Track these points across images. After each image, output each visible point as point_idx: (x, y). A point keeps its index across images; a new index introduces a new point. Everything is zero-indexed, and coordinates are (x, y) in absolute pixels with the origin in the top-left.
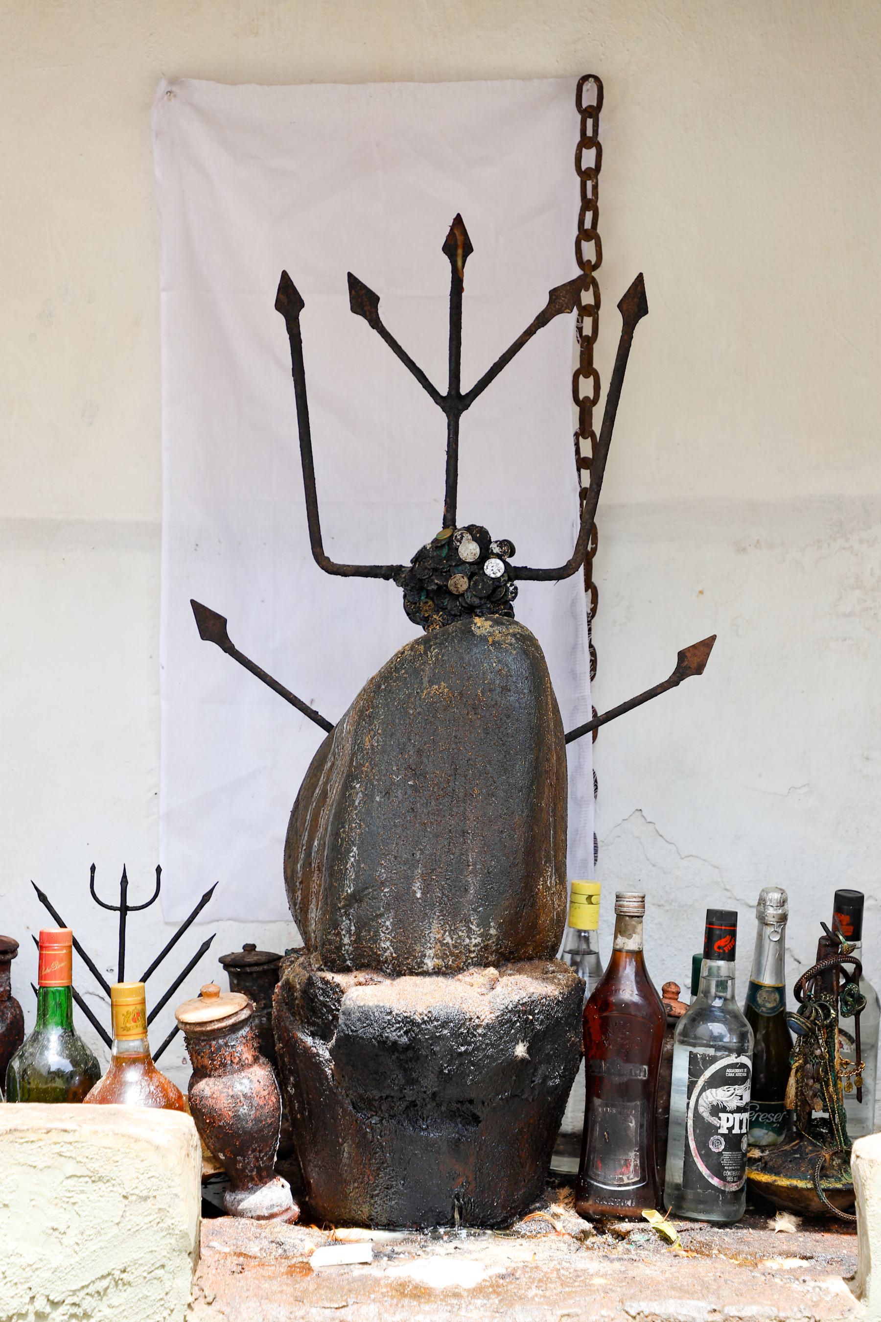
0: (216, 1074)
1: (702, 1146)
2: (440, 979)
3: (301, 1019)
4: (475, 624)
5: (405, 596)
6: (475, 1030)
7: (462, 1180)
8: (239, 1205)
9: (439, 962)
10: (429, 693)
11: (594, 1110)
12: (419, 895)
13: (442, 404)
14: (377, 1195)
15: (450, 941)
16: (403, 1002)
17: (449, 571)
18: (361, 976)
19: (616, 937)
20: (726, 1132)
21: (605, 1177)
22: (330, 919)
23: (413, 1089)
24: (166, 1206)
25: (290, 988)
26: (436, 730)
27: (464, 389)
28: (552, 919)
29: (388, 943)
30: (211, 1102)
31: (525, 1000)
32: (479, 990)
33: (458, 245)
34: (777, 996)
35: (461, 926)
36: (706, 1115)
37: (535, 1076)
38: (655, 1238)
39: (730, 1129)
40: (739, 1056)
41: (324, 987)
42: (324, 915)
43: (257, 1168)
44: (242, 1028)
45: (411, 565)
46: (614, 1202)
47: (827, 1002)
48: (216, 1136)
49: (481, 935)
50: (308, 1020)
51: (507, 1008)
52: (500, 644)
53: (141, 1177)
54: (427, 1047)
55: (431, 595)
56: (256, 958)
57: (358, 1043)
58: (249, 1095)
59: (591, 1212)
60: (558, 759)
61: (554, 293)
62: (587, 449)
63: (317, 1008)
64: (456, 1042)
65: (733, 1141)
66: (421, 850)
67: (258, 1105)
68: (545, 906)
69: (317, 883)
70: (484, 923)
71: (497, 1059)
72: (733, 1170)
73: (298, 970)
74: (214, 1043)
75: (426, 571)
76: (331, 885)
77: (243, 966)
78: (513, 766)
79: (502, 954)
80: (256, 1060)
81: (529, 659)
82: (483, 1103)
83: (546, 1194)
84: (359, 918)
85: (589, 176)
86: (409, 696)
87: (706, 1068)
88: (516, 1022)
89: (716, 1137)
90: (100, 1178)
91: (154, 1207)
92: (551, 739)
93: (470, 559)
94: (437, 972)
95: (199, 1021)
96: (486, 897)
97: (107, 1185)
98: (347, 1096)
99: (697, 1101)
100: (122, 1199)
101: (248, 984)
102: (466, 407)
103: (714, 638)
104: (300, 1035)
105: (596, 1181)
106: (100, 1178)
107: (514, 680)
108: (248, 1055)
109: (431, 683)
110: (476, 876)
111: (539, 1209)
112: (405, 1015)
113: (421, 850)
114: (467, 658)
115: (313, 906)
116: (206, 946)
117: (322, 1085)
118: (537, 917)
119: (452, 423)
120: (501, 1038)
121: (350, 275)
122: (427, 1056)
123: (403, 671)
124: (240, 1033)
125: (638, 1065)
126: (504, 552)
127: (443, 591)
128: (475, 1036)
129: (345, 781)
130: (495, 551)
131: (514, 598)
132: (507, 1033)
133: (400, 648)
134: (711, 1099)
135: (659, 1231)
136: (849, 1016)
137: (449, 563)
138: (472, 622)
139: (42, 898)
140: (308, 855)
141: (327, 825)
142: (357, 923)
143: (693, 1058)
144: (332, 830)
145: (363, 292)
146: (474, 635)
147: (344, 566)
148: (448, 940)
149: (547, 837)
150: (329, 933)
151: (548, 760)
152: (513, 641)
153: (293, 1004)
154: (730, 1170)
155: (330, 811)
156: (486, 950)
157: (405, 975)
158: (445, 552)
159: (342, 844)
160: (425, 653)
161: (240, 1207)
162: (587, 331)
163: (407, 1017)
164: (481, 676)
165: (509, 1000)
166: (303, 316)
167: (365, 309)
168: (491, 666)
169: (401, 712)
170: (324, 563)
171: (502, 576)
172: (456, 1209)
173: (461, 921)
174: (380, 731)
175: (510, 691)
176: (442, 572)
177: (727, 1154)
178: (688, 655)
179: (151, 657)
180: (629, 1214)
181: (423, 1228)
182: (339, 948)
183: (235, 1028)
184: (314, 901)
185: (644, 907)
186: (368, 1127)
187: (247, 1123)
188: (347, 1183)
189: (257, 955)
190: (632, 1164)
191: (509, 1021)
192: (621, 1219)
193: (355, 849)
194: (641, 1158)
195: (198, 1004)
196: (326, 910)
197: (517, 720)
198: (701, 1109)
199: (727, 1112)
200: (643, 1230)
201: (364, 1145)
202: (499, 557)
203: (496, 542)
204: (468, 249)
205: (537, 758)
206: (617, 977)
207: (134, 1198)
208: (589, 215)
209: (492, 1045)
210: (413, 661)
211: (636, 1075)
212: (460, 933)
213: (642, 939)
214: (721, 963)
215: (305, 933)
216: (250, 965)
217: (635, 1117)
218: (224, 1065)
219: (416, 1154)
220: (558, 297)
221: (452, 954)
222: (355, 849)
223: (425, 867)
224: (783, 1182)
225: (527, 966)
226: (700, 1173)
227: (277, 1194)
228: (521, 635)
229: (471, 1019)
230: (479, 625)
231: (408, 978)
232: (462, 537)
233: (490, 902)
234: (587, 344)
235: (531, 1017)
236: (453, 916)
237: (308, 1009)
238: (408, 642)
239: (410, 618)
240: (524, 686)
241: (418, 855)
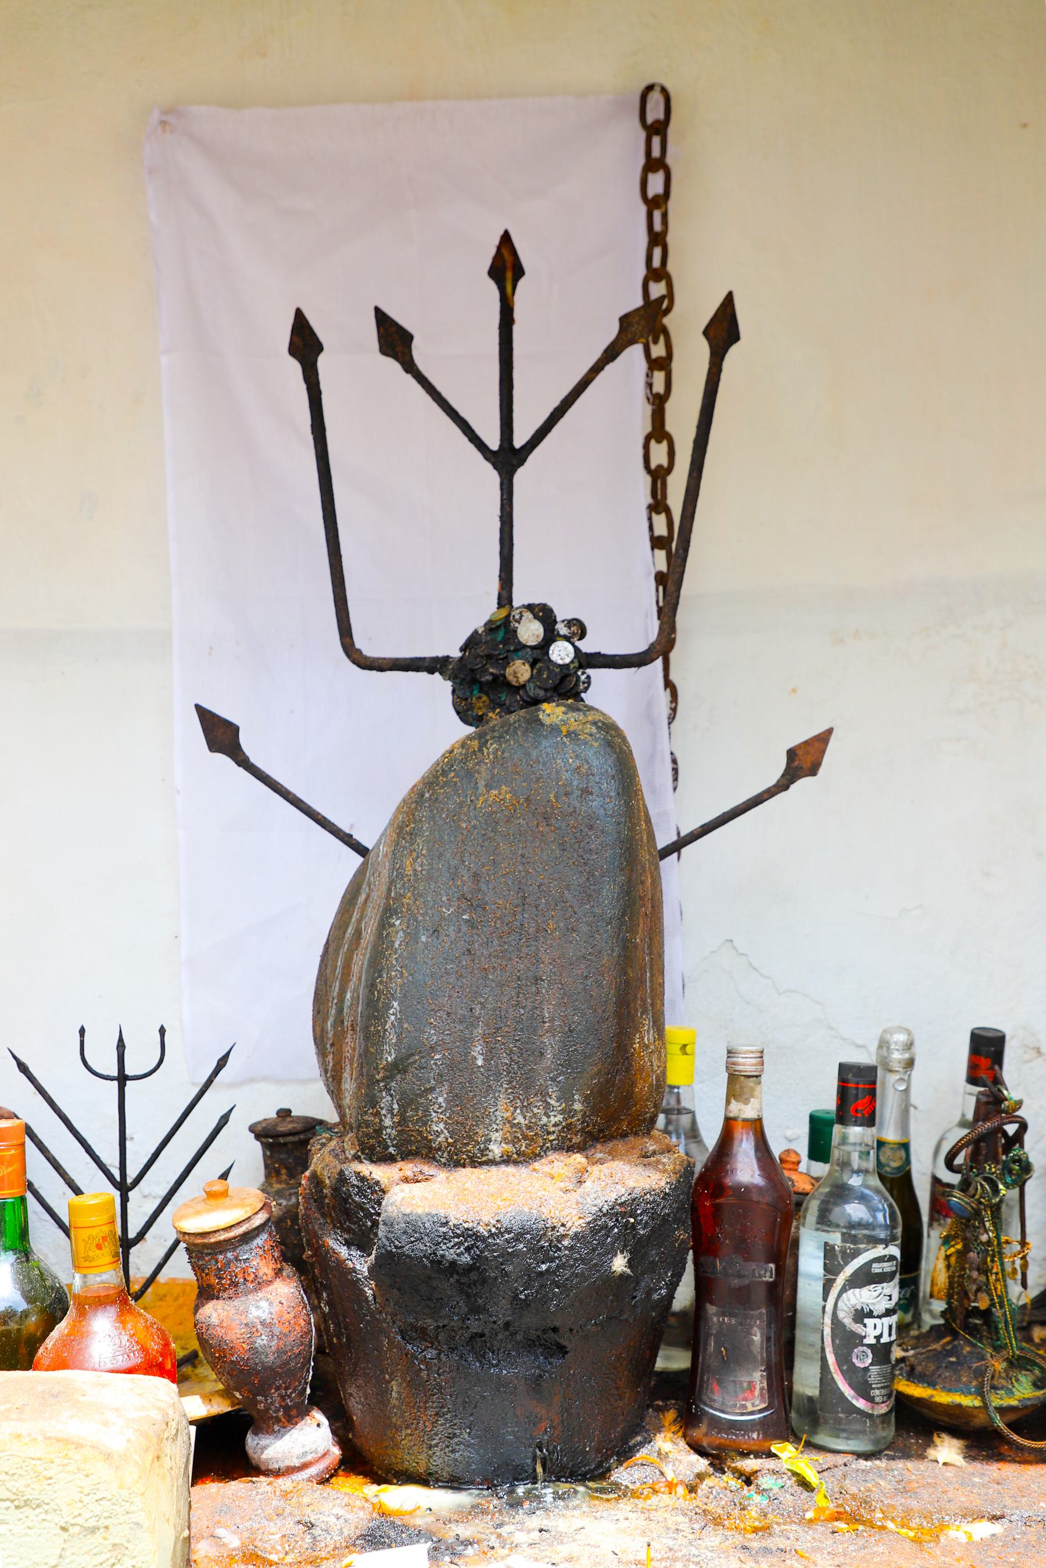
0: (226, 1295)
2: (510, 1169)
3: (332, 1222)
4: (544, 711)
5: (454, 692)
6: (560, 1242)
7: (545, 1424)
8: (262, 1453)
9: (509, 1148)
10: (486, 800)
14: (436, 1445)
15: (522, 1121)
16: (463, 1208)
17: (506, 657)
18: (409, 1168)
19: (728, 1102)
20: (873, 1341)
21: (723, 1404)
22: (367, 1095)
23: (479, 1319)
24: (123, 1541)
25: (318, 1183)
26: (497, 847)
27: (519, 441)
28: (651, 1085)
29: (442, 1126)
30: (220, 1332)
31: (623, 1199)
32: (562, 1185)
33: (506, 267)
34: (903, 1153)
35: (535, 1100)
36: (848, 1322)
37: (635, 1290)
38: (791, 1482)
39: (878, 1338)
42: (359, 1088)
43: (284, 1408)
44: (258, 1235)
46: (736, 1435)
47: (993, 1173)
49: (563, 1112)
50: (341, 1225)
51: (600, 1210)
52: (576, 735)
53: (86, 1500)
54: (497, 1268)
55: (486, 689)
56: (290, 1126)
58: (268, 1321)
59: (705, 1445)
60: (653, 882)
61: (625, 321)
62: (661, 529)
63: (352, 1211)
65: (881, 1352)
66: (481, 1003)
67: (281, 1333)
68: (642, 1069)
69: (352, 1045)
70: (566, 1096)
72: (882, 1388)
73: (329, 1158)
74: (220, 1257)
75: (478, 660)
76: (367, 1050)
77: (275, 1136)
78: (599, 892)
79: (590, 1133)
80: (278, 1273)
81: (615, 752)
82: (571, 1330)
83: (647, 1419)
84: (403, 1093)
85: (657, 203)
86: (461, 805)
87: (846, 1263)
88: (612, 1228)
89: (861, 1348)
90: (27, 1503)
91: (105, 1542)
92: (644, 856)
93: (532, 642)
94: (507, 1160)
95: (201, 1231)
96: (567, 1064)
97: (38, 1511)
98: (394, 1322)
100: (59, 1531)
101: (282, 1156)
102: (522, 462)
104: (331, 1243)
105: (712, 1408)
106: (27, 1503)
107: (597, 779)
108: (265, 1268)
109: (489, 787)
110: (554, 1036)
111: (641, 1444)
112: (466, 1225)
113: (481, 1003)
114: (534, 753)
115: (346, 1075)
117: (361, 1308)
118: (633, 1084)
119: (505, 481)
120: (594, 1250)
121: (377, 310)
122: (496, 1278)
123: (452, 774)
125: (762, 1264)
127: (500, 683)
128: (559, 1249)
129: (382, 916)
130: (562, 633)
131: (586, 689)
132: (602, 1244)
133: (448, 747)
134: (853, 1301)
135: (795, 1474)
136: (1014, 1188)
137: (507, 648)
139: (23, 1068)
140: (340, 1011)
141: (361, 973)
142: (400, 1100)
143: (829, 1251)
144: (366, 980)
146: (542, 725)
147: (379, 659)
148: (520, 1119)
149: (643, 982)
150: (366, 1112)
151: (642, 882)
152: (594, 730)
153: (322, 1203)
154: (878, 1389)
155: (364, 955)
156: (569, 1130)
157: (464, 1166)
158: (500, 635)
159: (379, 998)
160: (481, 750)
161: (264, 1456)
162: (659, 387)
163: (468, 1229)
164: (554, 776)
165: (604, 1199)
167: (397, 349)
168: (566, 763)
169: (451, 827)
170: (355, 656)
171: (572, 662)
172: (539, 1461)
173: (536, 1095)
174: (424, 852)
175: (592, 793)
176: (498, 659)
177: (874, 1369)
178: (800, 752)
179: (163, 780)
180: (754, 1448)
181: (496, 1486)
182: (379, 1132)
183: (247, 1238)
184: (348, 1068)
187: (266, 1357)
188: (398, 1429)
190: (758, 1387)
191: (604, 1227)
192: (745, 1455)
193: (396, 1004)
195: (200, 1206)
197: (603, 832)
198: (841, 1315)
200: (774, 1472)
201: (415, 1384)
202: (567, 639)
204: (519, 272)
205: (630, 880)
207: (77, 1529)
208: (657, 252)
210: (465, 760)
211: (760, 1276)
212: (535, 1110)
213: (761, 1104)
214: (858, 1129)
216: (284, 1135)
218: (236, 1285)
219: (484, 1397)
220: (630, 324)
221: (525, 1137)
222: (396, 1004)
223: (487, 1025)
224: (943, 1398)
225: (620, 1145)
226: (842, 1394)
227: (311, 1437)
228: (604, 723)
229: (553, 1228)
230: (548, 712)
232: (522, 616)
233: (573, 1068)
234: (658, 403)
235: (632, 1220)
236: (525, 1087)
238: (457, 739)
239: (461, 718)
240: (610, 787)
241: (477, 1010)
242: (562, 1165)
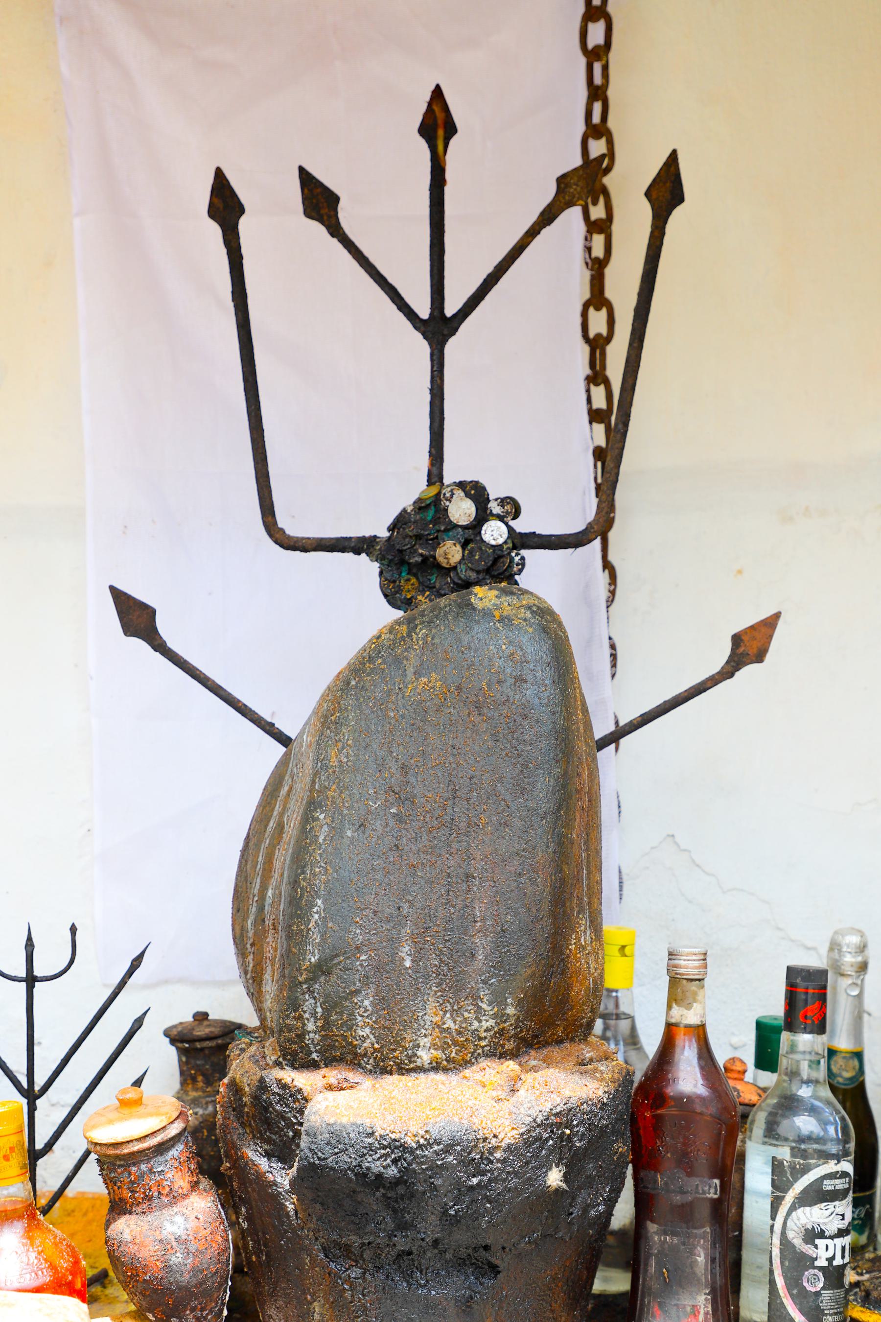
0: (139, 1210)
1: (794, 1283)
2: (440, 1077)
3: (252, 1132)
4: (476, 595)
5: (381, 573)
6: (491, 1154)
9: (439, 1054)
11: (647, 1238)
12: (408, 964)
13: (422, 328)
15: (452, 1025)
16: (389, 1118)
17: (437, 538)
18: (333, 1075)
19: (669, 1007)
20: (826, 1264)
25: (237, 1091)
27: (451, 308)
28: (588, 988)
29: (368, 1030)
30: (133, 1249)
31: (559, 1109)
32: (494, 1094)
33: (437, 125)
34: (856, 1063)
35: (467, 1004)
36: (798, 1242)
39: (830, 1260)
40: (839, 1162)
41: (281, 1092)
44: (173, 1146)
45: (387, 534)
48: (141, 1293)
49: (495, 1016)
51: (534, 1121)
52: (510, 620)
54: (425, 1181)
56: (207, 1030)
57: (328, 1175)
58: (183, 1237)
61: (562, 181)
63: (273, 1120)
64: (465, 1172)
65: (833, 1275)
67: (197, 1250)
68: (578, 971)
69: (274, 945)
70: (498, 1000)
71: (523, 1192)
72: (836, 1314)
73: (248, 1065)
75: (407, 540)
76: (289, 951)
77: (191, 1041)
79: (523, 1039)
80: (194, 1186)
81: (550, 638)
82: (504, 1248)
84: (327, 996)
85: (597, 55)
86: (389, 692)
87: (796, 1180)
88: (547, 1140)
89: (812, 1271)
92: (581, 747)
93: (464, 522)
94: (436, 1067)
95: (113, 1141)
98: (317, 1239)
99: (785, 1223)
101: (199, 1062)
102: (454, 331)
103: (777, 616)
107: (532, 667)
108: (181, 1181)
109: (417, 674)
112: (393, 1136)
114: (466, 639)
115: (267, 976)
116: (138, 1024)
118: (569, 988)
119: (436, 352)
120: (527, 1163)
121: (302, 170)
122: (424, 1193)
123: (380, 661)
124: (170, 1153)
125: (706, 1179)
126: (507, 512)
127: (430, 565)
128: (491, 1162)
129: (306, 809)
130: (495, 512)
131: (520, 571)
132: (536, 1156)
133: (375, 632)
134: (803, 1220)
137: (437, 527)
138: (471, 593)
140: (261, 908)
141: (283, 868)
142: (324, 1003)
143: (777, 1166)
144: (289, 877)
145: (319, 190)
146: (474, 609)
148: (449, 1024)
149: (579, 879)
152: (528, 615)
153: (241, 1111)
154: (831, 1315)
155: (287, 850)
156: (501, 1035)
158: (431, 514)
159: (302, 895)
160: (409, 635)
162: (598, 251)
163: (395, 1140)
164: (486, 662)
165: (538, 1109)
166: (244, 224)
167: (323, 212)
169: (378, 716)
171: (505, 542)
174: (350, 742)
175: (526, 682)
177: (827, 1293)
178: (745, 638)
179: (76, 666)
182: (301, 1036)
183: (162, 1148)
184: (269, 969)
185: (706, 968)
186: (345, 1282)
187: (181, 1275)
189: (209, 1026)
190: (702, 1312)
191: (539, 1138)
193: (319, 902)
194: (714, 1302)
196: (283, 985)
197: (537, 722)
198: (790, 1235)
199: (826, 1238)
202: (501, 518)
203: (496, 500)
204: (451, 129)
205: (566, 773)
206: (673, 1061)
208: (597, 107)
209: (516, 1174)
210: (392, 647)
211: (704, 1193)
212: (466, 1015)
213: (704, 1008)
215: (260, 1010)
216: (201, 1039)
217: (704, 1249)
218: (150, 1198)
220: (567, 185)
221: (455, 1043)
222: (319, 902)
223: (416, 925)
228: (538, 608)
229: (485, 1140)
230: (480, 595)
231: (395, 1077)
232: (453, 494)
233: (505, 971)
234: (597, 268)
235: (568, 1132)
236: (455, 990)
237: (260, 1119)
238: (385, 624)
239: (389, 602)
240: (545, 675)
241: (405, 909)
242: (494, 1072)
